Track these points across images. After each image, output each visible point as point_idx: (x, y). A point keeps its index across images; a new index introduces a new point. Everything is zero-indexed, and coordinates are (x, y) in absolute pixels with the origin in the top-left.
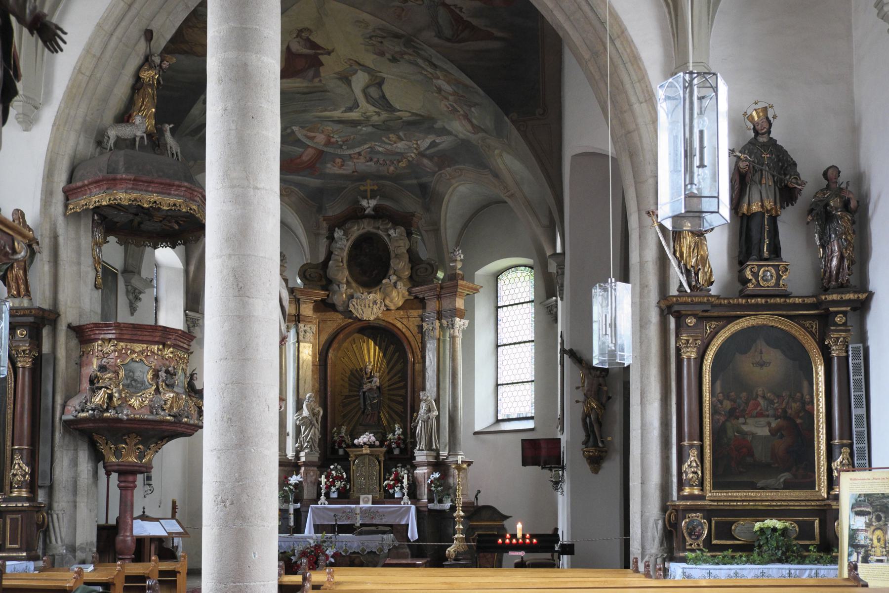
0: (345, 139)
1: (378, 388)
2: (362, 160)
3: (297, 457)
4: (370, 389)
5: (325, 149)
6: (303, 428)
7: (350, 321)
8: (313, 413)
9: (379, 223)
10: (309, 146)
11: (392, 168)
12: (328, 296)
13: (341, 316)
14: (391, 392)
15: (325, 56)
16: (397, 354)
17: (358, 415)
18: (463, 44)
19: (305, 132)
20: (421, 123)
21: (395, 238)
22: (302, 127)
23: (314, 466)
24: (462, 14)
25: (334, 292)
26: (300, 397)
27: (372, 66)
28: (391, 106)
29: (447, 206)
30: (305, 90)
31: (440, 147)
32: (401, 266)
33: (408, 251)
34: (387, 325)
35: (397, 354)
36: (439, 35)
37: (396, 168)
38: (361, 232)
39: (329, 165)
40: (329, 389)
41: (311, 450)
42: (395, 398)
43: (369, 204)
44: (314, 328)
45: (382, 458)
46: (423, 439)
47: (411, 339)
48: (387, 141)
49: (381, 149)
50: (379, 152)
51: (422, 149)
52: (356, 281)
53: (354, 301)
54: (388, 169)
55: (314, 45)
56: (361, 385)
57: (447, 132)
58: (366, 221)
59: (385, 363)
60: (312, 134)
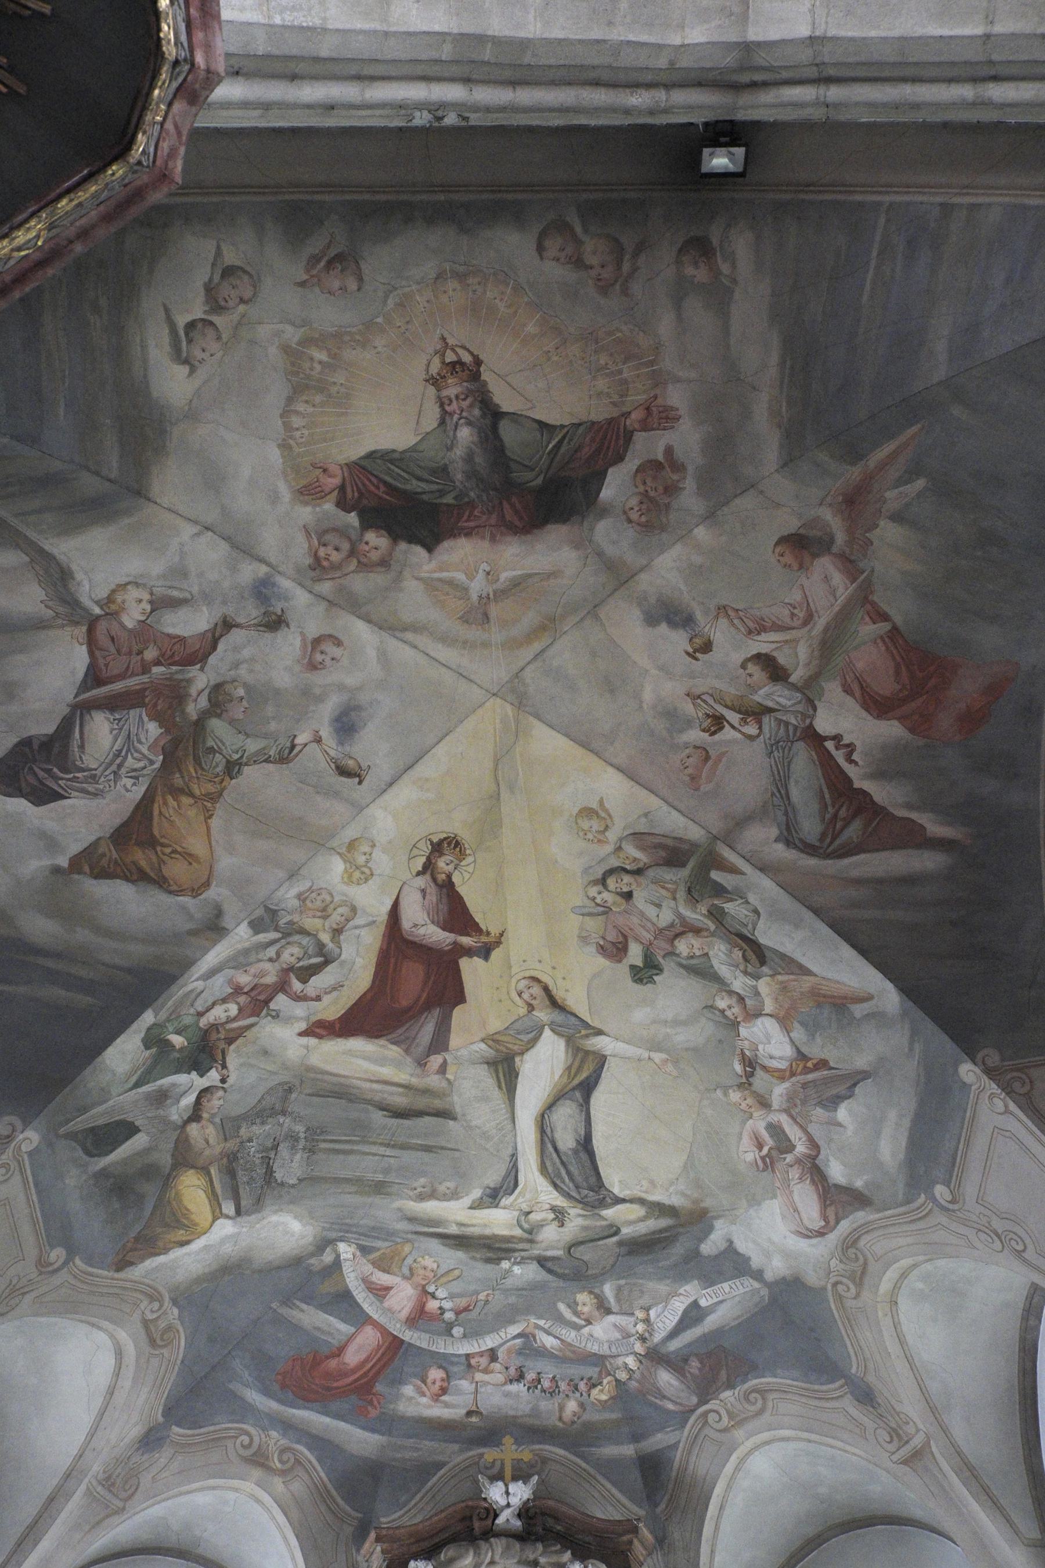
0: (462, 1302)
5: (408, 1336)
10: (368, 1320)
18: (846, 861)
19: (368, 1268)
20: (674, 1241)
22: (364, 1250)
28: (599, 1185)
30: (400, 1100)
31: (711, 1322)
36: (789, 837)
37: (582, 1405)
39: (408, 1390)
43: (509, 1497)
48: (568, 1314)
49: (549, 1342)
50: (542, 1353)
51: (658, 1337)
54: (561, 1408)
55: (456, 914)
57: (733, 1264)
60: (382, 1278)
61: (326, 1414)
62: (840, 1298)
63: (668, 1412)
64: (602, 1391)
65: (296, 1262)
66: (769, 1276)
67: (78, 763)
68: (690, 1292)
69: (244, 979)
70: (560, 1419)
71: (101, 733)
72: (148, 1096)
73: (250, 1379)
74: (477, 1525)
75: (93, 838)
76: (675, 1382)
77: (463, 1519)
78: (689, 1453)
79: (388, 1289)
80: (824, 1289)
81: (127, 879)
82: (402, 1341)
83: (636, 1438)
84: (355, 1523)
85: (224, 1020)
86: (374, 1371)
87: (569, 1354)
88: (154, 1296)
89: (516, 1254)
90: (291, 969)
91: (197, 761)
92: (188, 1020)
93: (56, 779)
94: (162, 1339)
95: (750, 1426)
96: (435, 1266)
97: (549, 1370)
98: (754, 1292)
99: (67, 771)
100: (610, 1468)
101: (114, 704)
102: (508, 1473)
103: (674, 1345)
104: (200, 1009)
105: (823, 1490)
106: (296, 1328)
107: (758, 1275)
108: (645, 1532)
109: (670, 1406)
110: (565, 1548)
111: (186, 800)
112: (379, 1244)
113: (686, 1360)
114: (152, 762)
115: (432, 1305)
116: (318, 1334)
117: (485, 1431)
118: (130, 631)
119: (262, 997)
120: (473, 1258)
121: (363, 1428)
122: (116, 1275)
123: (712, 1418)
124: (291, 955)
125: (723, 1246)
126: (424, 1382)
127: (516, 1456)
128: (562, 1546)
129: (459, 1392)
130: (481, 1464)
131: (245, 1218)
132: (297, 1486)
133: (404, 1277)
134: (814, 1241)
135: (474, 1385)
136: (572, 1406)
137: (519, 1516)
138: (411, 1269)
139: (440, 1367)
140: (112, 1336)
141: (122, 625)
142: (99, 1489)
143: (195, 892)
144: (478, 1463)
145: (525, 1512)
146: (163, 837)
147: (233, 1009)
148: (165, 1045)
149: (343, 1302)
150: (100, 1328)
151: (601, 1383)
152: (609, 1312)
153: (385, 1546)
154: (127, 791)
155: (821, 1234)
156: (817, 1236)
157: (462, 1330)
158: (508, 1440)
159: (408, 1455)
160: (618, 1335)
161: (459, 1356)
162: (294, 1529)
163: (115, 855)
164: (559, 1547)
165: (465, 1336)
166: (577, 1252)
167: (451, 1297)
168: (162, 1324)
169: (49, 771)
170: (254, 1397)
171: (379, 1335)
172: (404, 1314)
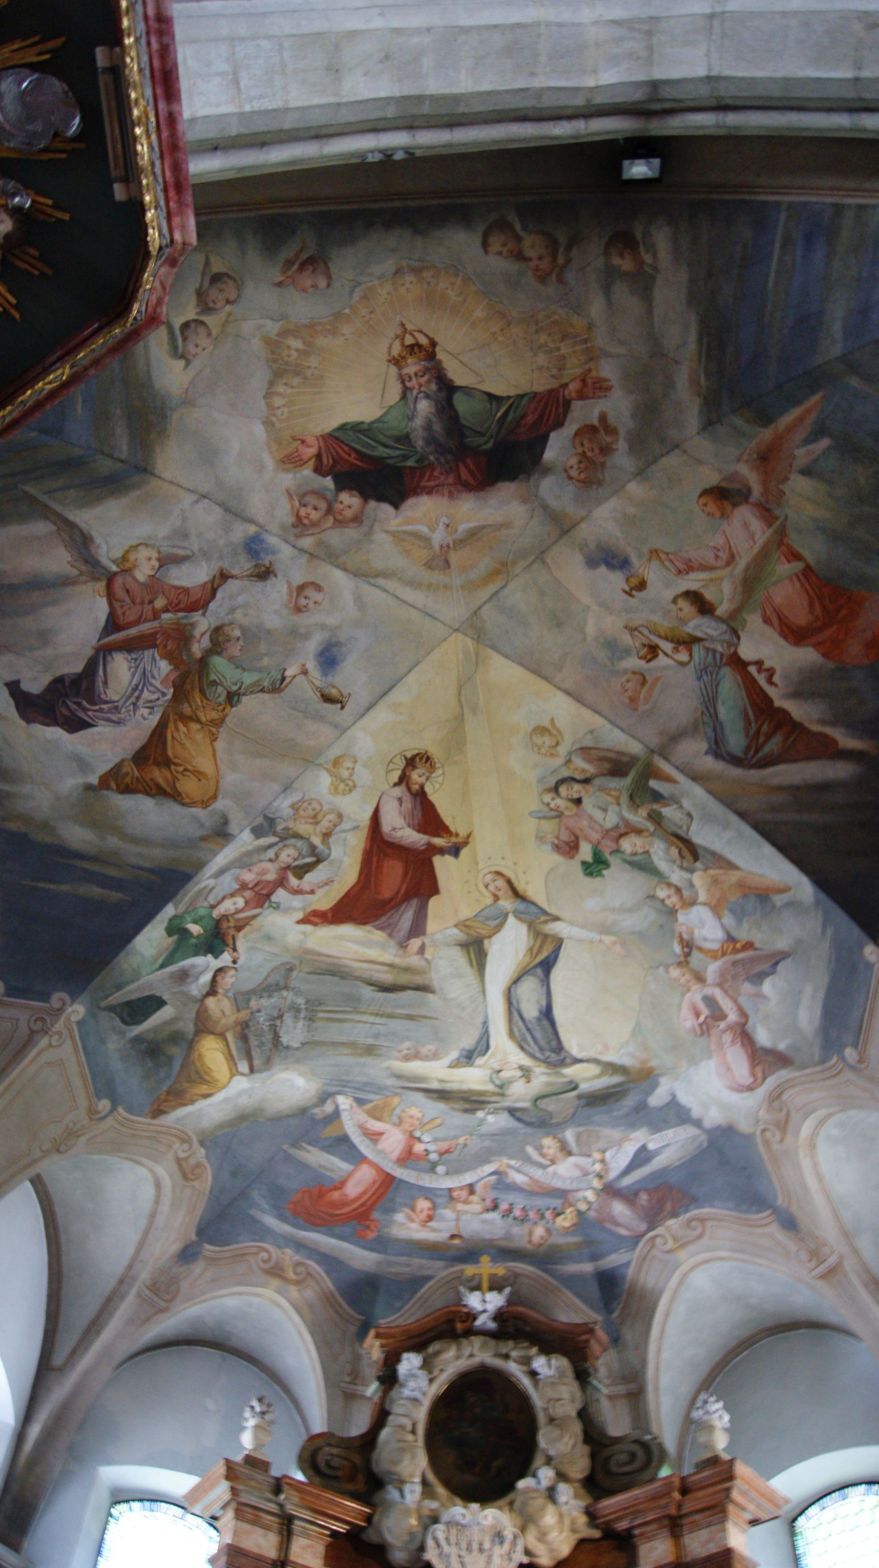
0: (444, 1146)
2: (475, 1206)
5: (399, 1173)
9: (507, 1346)
11: (539, 1232)
12: (369, 1519)
15: (448, 858)
20: (623, 1095)
21: (543, 1376)
22: (360, 1102)
24: (771, 691)
27: (541, 899)
28: (559, 1048)
29: (662, 1332)
30: (387, 977)
31: (657, 1163)
32: (560, 1443)
36: (717, 750)
37: (548, 1231)
39: (400, 1217)
43: (485, 1304)
49: (519, 1179)
50: (514, 1188)
51: (612, 1175)
52: (447, 1483)
53: (439, 1530)
54: (531, 1233)
55: (429, 819)
57: (676, 1114)
58: (477, 1341)
60: (375, 1125)
62: (767, 1143)
63: (622, 1237)
64: (565, 1219)
66: (707, 1124)
67: (103, 696)
68: (639, 1137)
69: (249, 877)
70: (530, 1242)
71: (121, 671)
72: (172, 975)
73: (267, 1207)
74: (459, 1326)
75: (117, 760)
79: (381, 1134)
81: (148, 794)
83: (594, 1258)
85: (233, 911)
87: (537, 1189)
88: (185, 1139)
89: (490, 1106)
90: (288, 867)
91: (203, 692)
92: (202, 912)
93: (85, 710)
95: (691, 1248)
97: (519, 1202)
98: (695, 1138)
99: (93, 703)
101: (130, 646)
102: (485, 1285)
103: (627, 1181)
104: (212, 902)
106: (304, 1166)
107: (698, 1123)
108: (601, 1333)
109: (623, 1232)
110: (533, 1344)
111: (194, 726)
113: (636, 1194)
114: (164, 695)
115: (419, 1148)
118: (142, 584)
119: (264, 892)
120: (453, 1109)
123: (659, 1241)
124: (288, 855)
125: (667, 1099)
126: (413, 1210)
127: (493, 1271)
129: (443, 1219)
133: (395, 1125)
140: (152, 1171)
141: (135, 579)
143: (205, 804)
145: (499, 1316)
146: (176, 757)
147: (240, 902)
148: (184, 933)
149: (342, 1145)
152: (570, 1153)
153: (384, 1341)
154: (144, 719)
158: (485, 1259)
160: (577, 1173)
163: (136, 774)
165: (447, 1173)
166: (542, 1104)
167: (435, 1140)
168: (192, 1162)
169: (78, 704)
170: (271, 1221)
172: (395, 1155)
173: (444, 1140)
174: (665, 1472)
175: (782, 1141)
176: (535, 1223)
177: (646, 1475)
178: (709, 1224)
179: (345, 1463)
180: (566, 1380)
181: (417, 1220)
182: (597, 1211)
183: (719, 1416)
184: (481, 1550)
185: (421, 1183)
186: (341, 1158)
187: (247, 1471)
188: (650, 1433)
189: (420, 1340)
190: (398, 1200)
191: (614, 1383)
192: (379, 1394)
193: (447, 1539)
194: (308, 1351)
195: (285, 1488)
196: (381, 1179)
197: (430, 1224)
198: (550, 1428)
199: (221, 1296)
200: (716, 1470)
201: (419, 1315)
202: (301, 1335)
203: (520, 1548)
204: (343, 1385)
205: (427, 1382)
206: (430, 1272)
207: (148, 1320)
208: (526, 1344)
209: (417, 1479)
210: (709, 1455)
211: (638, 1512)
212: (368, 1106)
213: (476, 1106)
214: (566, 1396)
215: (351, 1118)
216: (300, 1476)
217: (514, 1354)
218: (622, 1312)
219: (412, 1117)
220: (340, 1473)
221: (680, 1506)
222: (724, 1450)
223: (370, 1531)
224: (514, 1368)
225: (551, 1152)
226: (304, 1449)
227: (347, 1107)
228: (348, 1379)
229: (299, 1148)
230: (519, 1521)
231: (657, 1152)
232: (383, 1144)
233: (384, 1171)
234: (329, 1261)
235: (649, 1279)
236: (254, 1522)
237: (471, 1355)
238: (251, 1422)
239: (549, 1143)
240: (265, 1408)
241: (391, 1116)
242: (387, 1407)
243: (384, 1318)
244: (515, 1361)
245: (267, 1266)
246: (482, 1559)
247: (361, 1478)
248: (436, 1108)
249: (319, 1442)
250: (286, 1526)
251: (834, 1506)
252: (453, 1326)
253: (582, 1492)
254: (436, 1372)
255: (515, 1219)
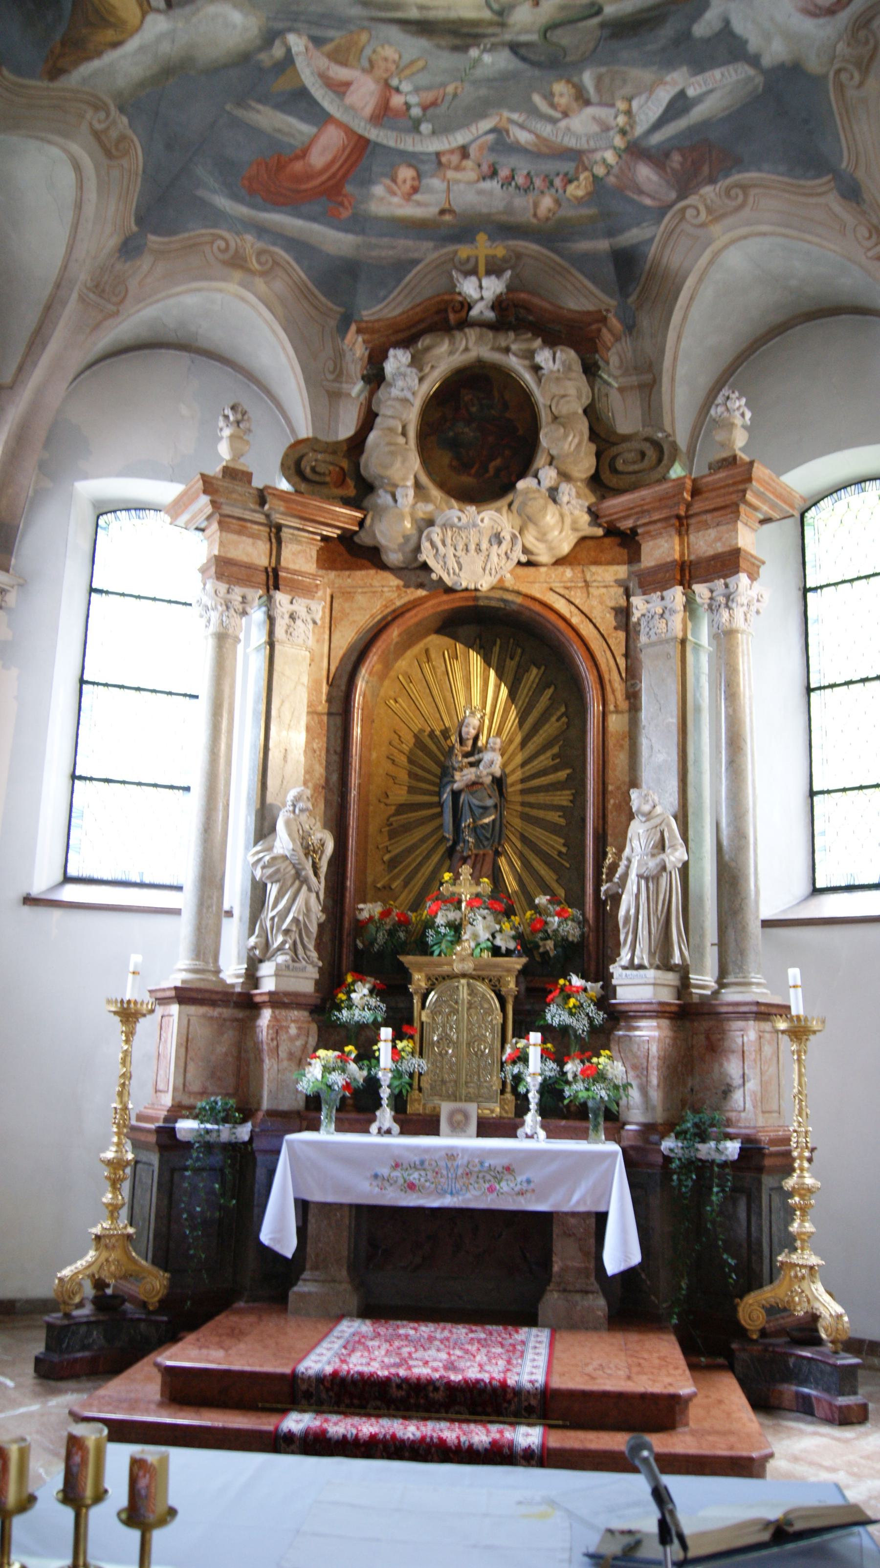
0: (429, 97)
1: (499, 782)
3: (252, 978)
4: (474, 785)
5: (374, 134)
6: (273, 890)
7: (422, 593)
8: (309, 850)
9: (508, 339)
12: (361, 523)
13: (394, 581)
14: (531, 799)
16: (550, 692)
17: (436, 858)
19: (323, 62)
21: (551, 377)
22: (317, 42)
23: (299, 1006)
25: (380, 511)
26: (269, 799)
29: (685, 318)
31: (697, 114)
32: (566, 445)
33: (585, 411)
34: (529, 603)
35: (550, 692)
37: (558, 202)
38: (458, 359)
39: (378, 190)
40: (354, 780)
41: (295, 959)
42: (540, 814)
43: (482, 291)
44: (319, 609)
45: (511, 985)
46: (642, 932)
47: (596, 645)
49: (523, 137)
50: (517, 149)
51: (639, 130)
52: (442, 486)
53: (436, 533)
54: (536, 205)
56: (446, 773)
58: (472, 334)
59: (513, 714)
60: (341, 73)
61: (300, 216)
62: (841, 88)
63: (645, 207)
64: (578, 187)
65: (244, 59)
66: (767, 61)
68: (678, 80)
70: (535, 215)
73: (217, 186)
74: (452, 317)
76: (654, 177)
77: (438, 312)
78: (664, 246)
79: (348, 84)
80: (825, 77)
82: (367, 141)
83: (611, 233)
84: (338, 316)
86: (341, 173)
87: (544, 149)
88: (98, 106)
89: (486, 40)
94: (117, 149)
95: (729, 221)
96: (396, 57)
97: (523, 167)
98: (750, 79)
100: (584, 263)
102: (482, 268)
103: (657, 138)
105: (794, 283)
106: (254, 131)
107: (754, 61)
108: (614, 322)
109: (648, 202)
110: (536, 335)
112: (331, 33)
113: (667, 155)
115: (397, 101)
116: (278, 136)
117: (458, 229)
120: (439, 47)
121: (338, 229)
122: (51, 85)
123: (690, 213)
125: (717, 26)
126: (394, 180)
127: (491, 252)
128: (533, 335)
129: (430, 190)
130: (456, 260)
131: (177, 12)
132: (279, 285)
133: (363, 70)
134: (822, 21)
135: (446, 184)
136: (547, 202)
137: (493, 308)
138: (371, 62)
139: (410, 165)
140: (65, 151)
142: (91, 295)
144: (453, 260)
145: (498, 305)
149: (299, 100)
150: (49, 142)
151: (577, 179)
152: (587, 103)
153: (366, 337)
155: (831, 12)
156: (825, 15)
157: (430, 126)
158: (482, 238)
159: (384, 253)
160: (596, 128)
161: (429, 154)
162: (281, 324)
164: (530, 335)
165: (434, 133)
166: (556, 36)
167: (417, 90)
168: (114, 134)
170: (223, 202)
171: (343, 134)
172: (368, 111)
173: (428, 88)
174: (677, 471)
175: (861, 84)
176: (542, 192)
177: (656, 475)
178: (753, 192)
179: (331, 468)
180: (573, 375)
181: (399, 192)
182: (617, 177)
183: (738, 410)
184: (478, 549)
185: (401, 146)
186: (302, 119)
187: (225, 484)
188: (662, 430)
189: (410, 334)
190: (375, 169)
191: (626, 373)
192: (366, 394)
193: (444, 543)
194: (284, 348)
195: (269, 498)
196: (352, 144)
197: (417, 197)
198: (553, 427)
199: (178, 294)
200: (731, 472)
201: (407, 305)
202: (274, 332)
203: (519, 548)
204: (325, 383)
205: (417, 381)
206: (416, 255)
207: (97, 327)
208: (530, 335)
209: (410, 483)
210: (725, 454)
211: (643, 512)
212: (329, 47)
213: (469, 41)
214: (572, 392)
215: (309, 66)
216: (284, 485)
217: (514, 347)
218: (638, 297)
219: (386, 59)
220: (328, 479)
221: (689, 506)
222: (742, 449)
223: (362, 534)
224: (515, 363)
225: (563, 101)
226: (286, 456)
227: (302, 48)
228: (331, 377)
229: (248, 107)
230: (518, 522)
231: (699, 99)
232: (354, 97)
233: (354, 133)
234: (299, 247)
235: (674, 258)
236: (241, 532)
237: (467, 349)
238: (227, 432)
239: (561, 90)
240: (239, 417)
241: (359, 60)
242: (374, 408)
243: (366, 308)
244: (515, 355)
245: (226, 257)
246: (479, 560)
247: (350, 483)
248: (415, 47)
249: (302, 449)
250: (276, 533)
251: (850, 497)
252: (446, 316)
253: (587, 491)
254: (427, 369)
255: (518, 187)
